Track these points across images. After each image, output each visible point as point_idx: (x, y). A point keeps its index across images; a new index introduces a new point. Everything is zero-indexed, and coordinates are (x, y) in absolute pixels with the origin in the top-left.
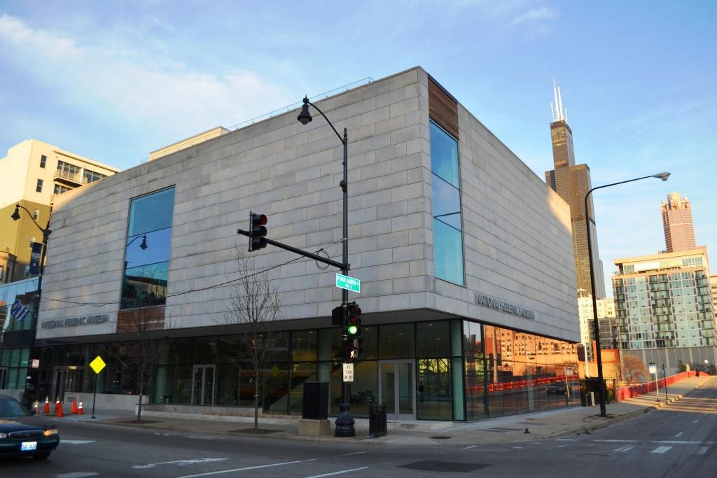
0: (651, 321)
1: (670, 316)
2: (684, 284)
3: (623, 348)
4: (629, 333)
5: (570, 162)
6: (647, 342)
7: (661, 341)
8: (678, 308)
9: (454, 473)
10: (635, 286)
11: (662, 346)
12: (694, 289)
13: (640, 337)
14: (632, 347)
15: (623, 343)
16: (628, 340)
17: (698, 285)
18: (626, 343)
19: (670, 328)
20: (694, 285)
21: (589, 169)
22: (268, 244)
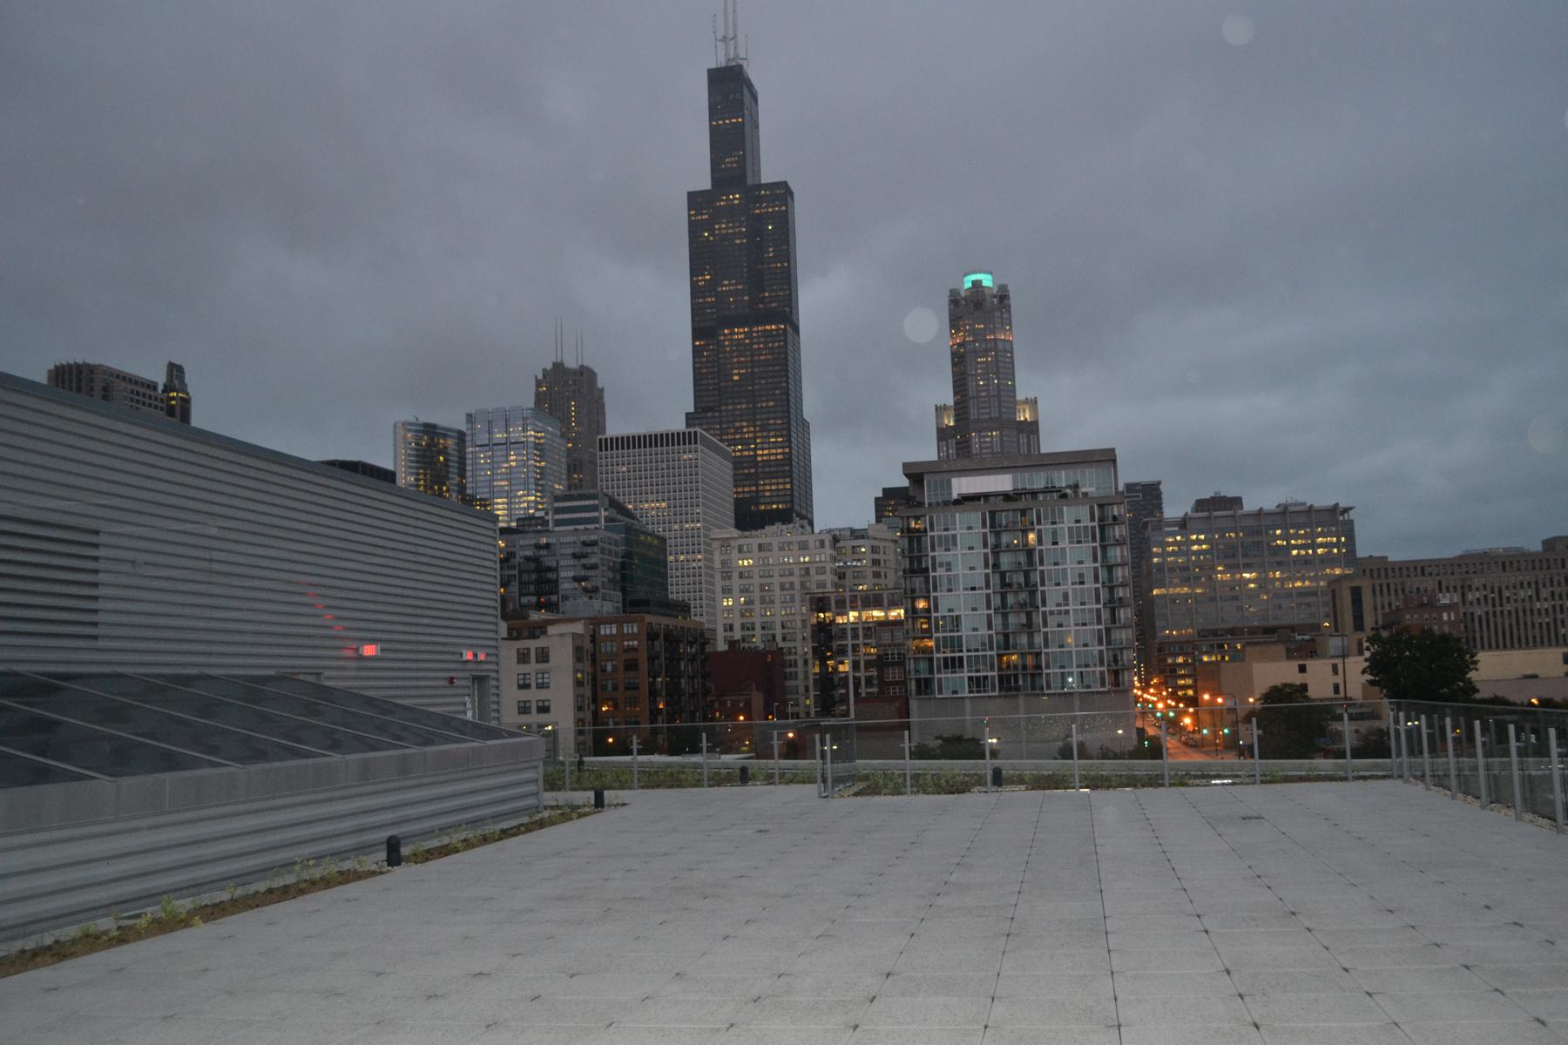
0: (988, 586)
1: (1032, 575)
2: (1071, 536)
3: (919, 693)
4: (936, 655)
5: (749, 174)
6: (978, 678)
7: (1008, 677)
8: (1053, 594)
9: (661, 792)
10: (954, 536)
11: (1009, 689)
12: (1094, 548)
13: (961, 666)
14: (940, 691)
15: (918, 681)
16: (931, 672)
17: (1103, 539)
18: (926, 680)
19: (1031, 645)
20: (1094, 539)
21: (791, 194)
22: (42, 378)
